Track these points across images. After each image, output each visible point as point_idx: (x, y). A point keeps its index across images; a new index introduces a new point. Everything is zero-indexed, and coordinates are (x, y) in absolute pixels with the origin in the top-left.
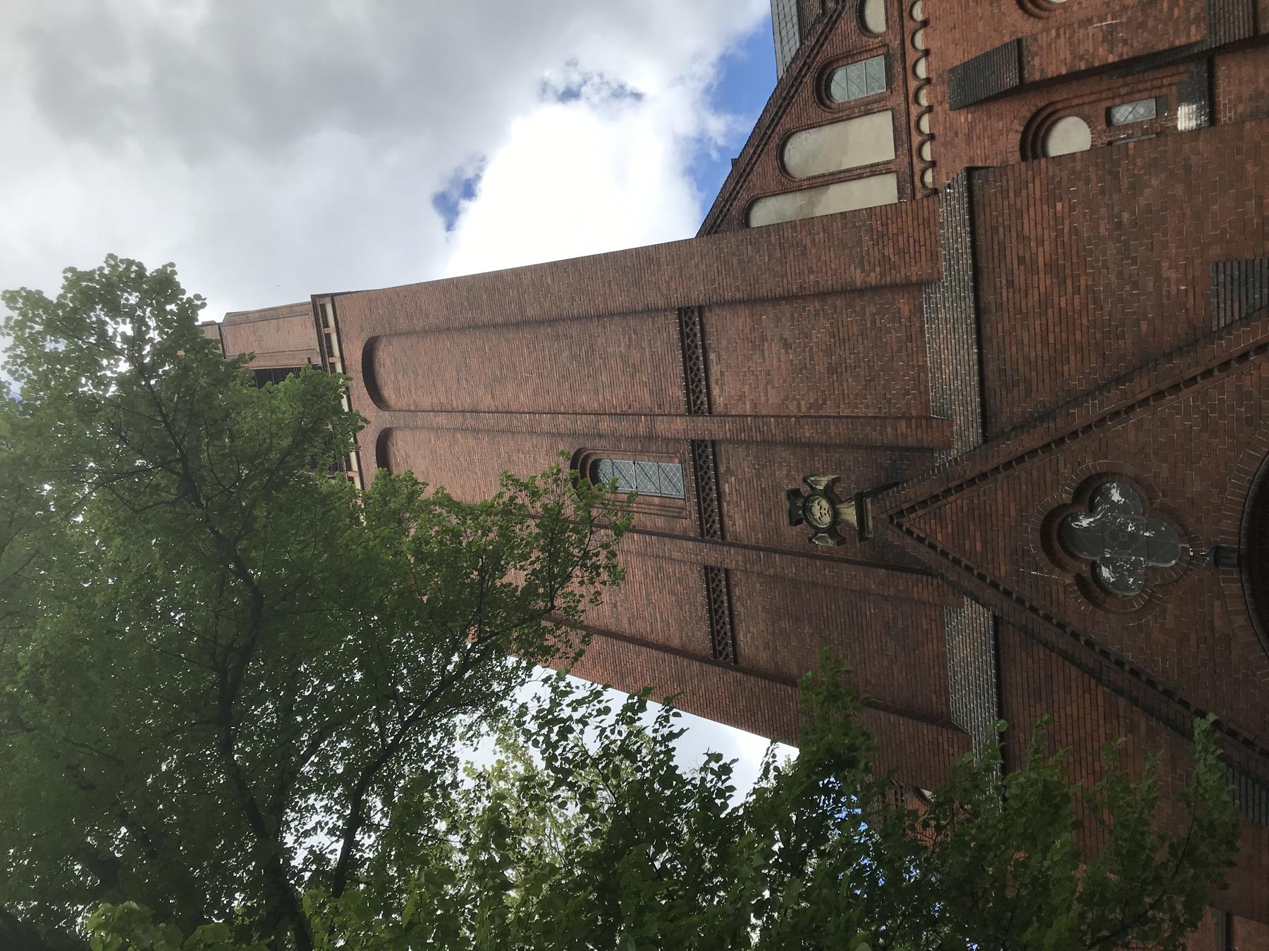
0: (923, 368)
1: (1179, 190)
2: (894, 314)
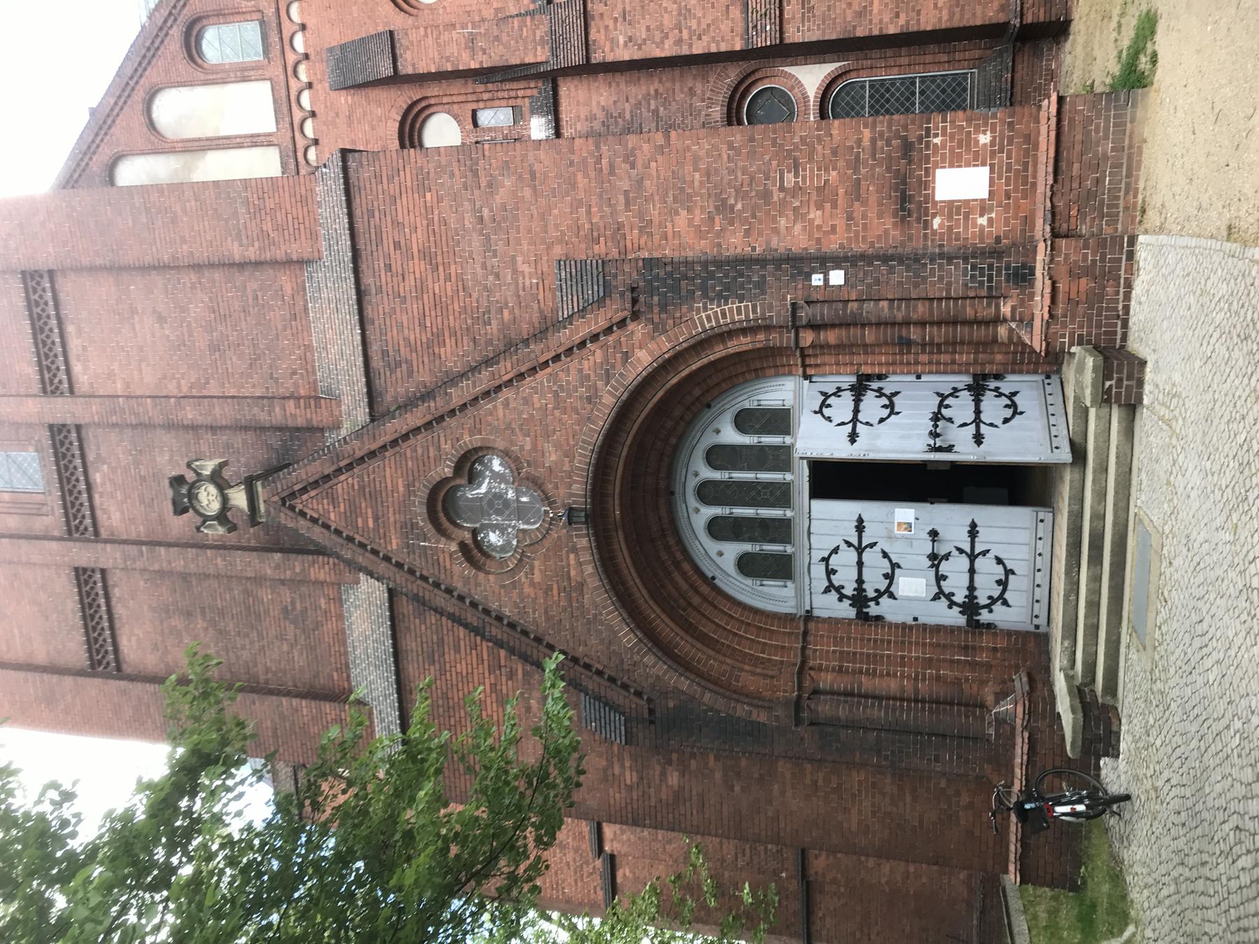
0: (308, 347)
1: (527, 193)
2: (277, 291)
